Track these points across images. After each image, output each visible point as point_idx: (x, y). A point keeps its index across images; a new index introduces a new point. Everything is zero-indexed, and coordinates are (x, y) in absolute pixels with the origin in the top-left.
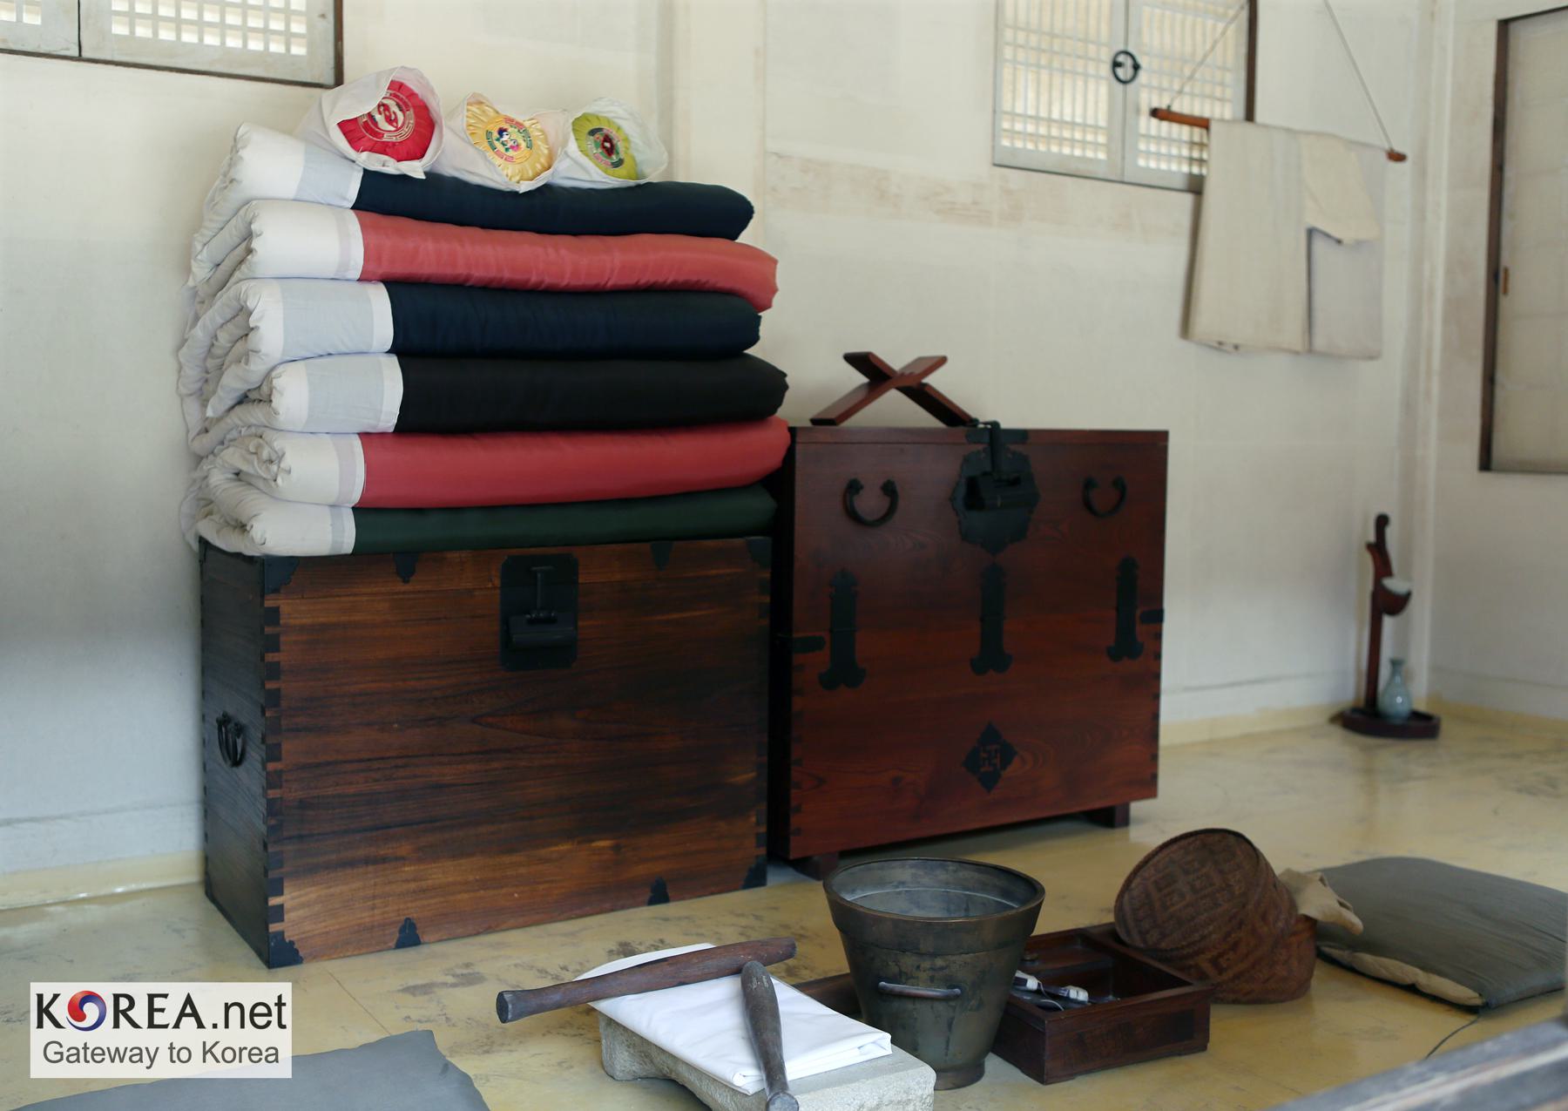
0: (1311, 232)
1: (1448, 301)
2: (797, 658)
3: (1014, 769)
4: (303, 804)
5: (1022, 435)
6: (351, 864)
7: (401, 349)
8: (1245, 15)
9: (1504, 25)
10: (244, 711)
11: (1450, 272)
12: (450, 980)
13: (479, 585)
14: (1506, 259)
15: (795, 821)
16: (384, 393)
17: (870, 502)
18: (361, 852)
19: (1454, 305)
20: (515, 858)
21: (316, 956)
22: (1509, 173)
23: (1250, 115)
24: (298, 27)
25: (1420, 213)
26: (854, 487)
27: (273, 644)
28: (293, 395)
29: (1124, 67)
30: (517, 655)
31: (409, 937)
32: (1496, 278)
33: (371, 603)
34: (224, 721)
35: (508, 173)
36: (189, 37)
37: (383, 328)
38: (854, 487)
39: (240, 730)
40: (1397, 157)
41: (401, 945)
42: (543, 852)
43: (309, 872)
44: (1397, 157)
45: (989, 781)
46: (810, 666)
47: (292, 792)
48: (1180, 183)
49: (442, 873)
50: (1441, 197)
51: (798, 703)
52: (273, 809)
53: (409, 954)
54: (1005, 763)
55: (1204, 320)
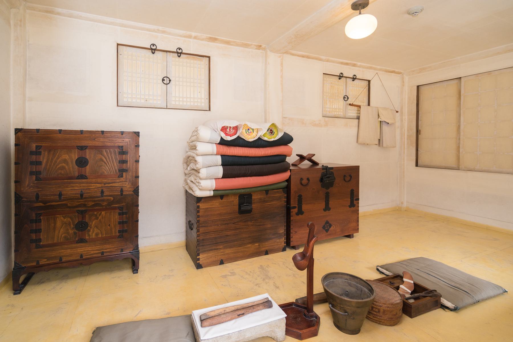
0: (118, 45)
1: (408, 136)
2: (292, 210)
3: (332, 228)
4: (203, 240)
5: (332, 168)
6: (212, 250)
7: (223, 165)
8: (367, 87)
9: (418, 87)
10: (194, 221)
11: (408, 130)
12: (230, 274)
13: (236, 200)
14: (420, 128)
15: (291, 239)
16: (220, 171)
17: (305, 182)
18: (214, 248)
19: (409, 137)
20: (242, 248)
21: (205, 267)
22: (420, 113)
23: (369, 105)
24: (203, 101)
25: (402, 120)
26: (302, 179)
27: (198, 212)
28: (203, 172)
29: (346, 98)
30: (241, 212)
31: (222, 263)
32: (418, 132)
33: (216, 203)
34: (190, 222)
35: (251, 138)
36: (185, 103)
37: (220, 162)
38: (302, 179)
39: (192, 224)
40: (397, 112)
41: (220, 264)
42: (246, 246)
43: (204, 252)
44: (397, 112)
45: (327, 231)
46: (294, 211)
47: (201, 238)
48: (356, 117)
49: (228, 251)
50: (406, 117)
51: (292, 218)
52: (198, 241)
53: (222, 266)
54: (330, 227)
55: (360, 140)
